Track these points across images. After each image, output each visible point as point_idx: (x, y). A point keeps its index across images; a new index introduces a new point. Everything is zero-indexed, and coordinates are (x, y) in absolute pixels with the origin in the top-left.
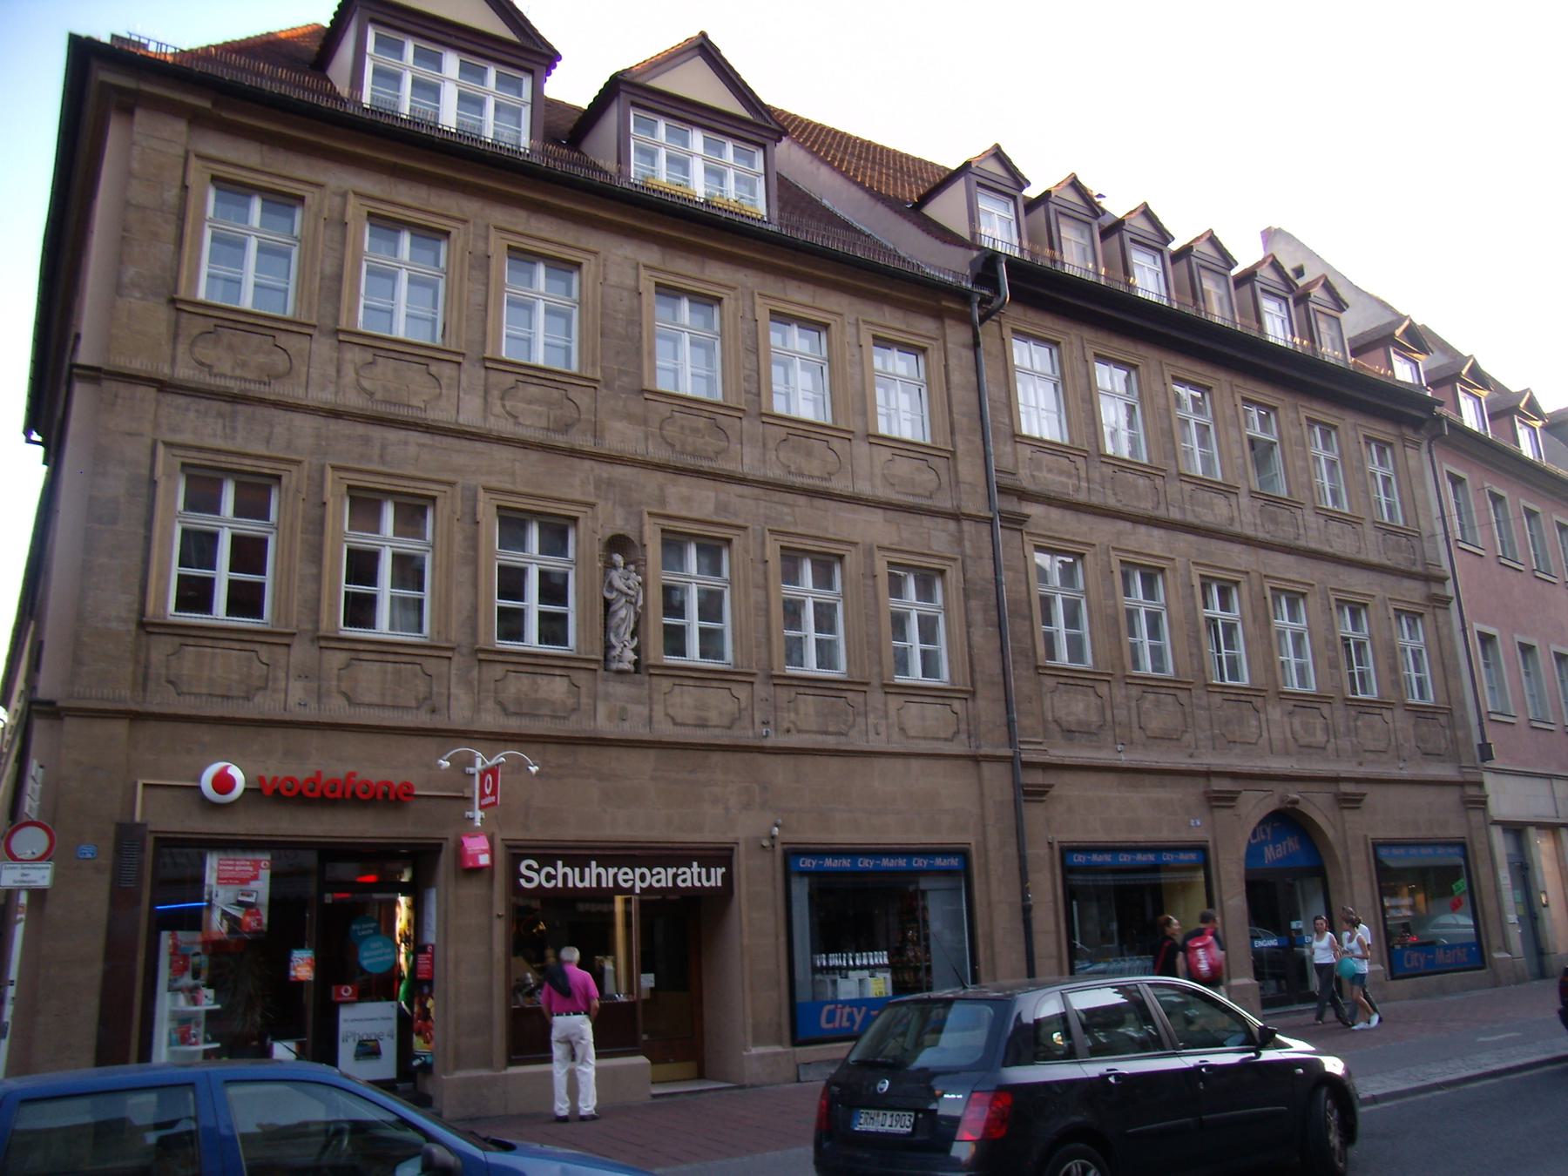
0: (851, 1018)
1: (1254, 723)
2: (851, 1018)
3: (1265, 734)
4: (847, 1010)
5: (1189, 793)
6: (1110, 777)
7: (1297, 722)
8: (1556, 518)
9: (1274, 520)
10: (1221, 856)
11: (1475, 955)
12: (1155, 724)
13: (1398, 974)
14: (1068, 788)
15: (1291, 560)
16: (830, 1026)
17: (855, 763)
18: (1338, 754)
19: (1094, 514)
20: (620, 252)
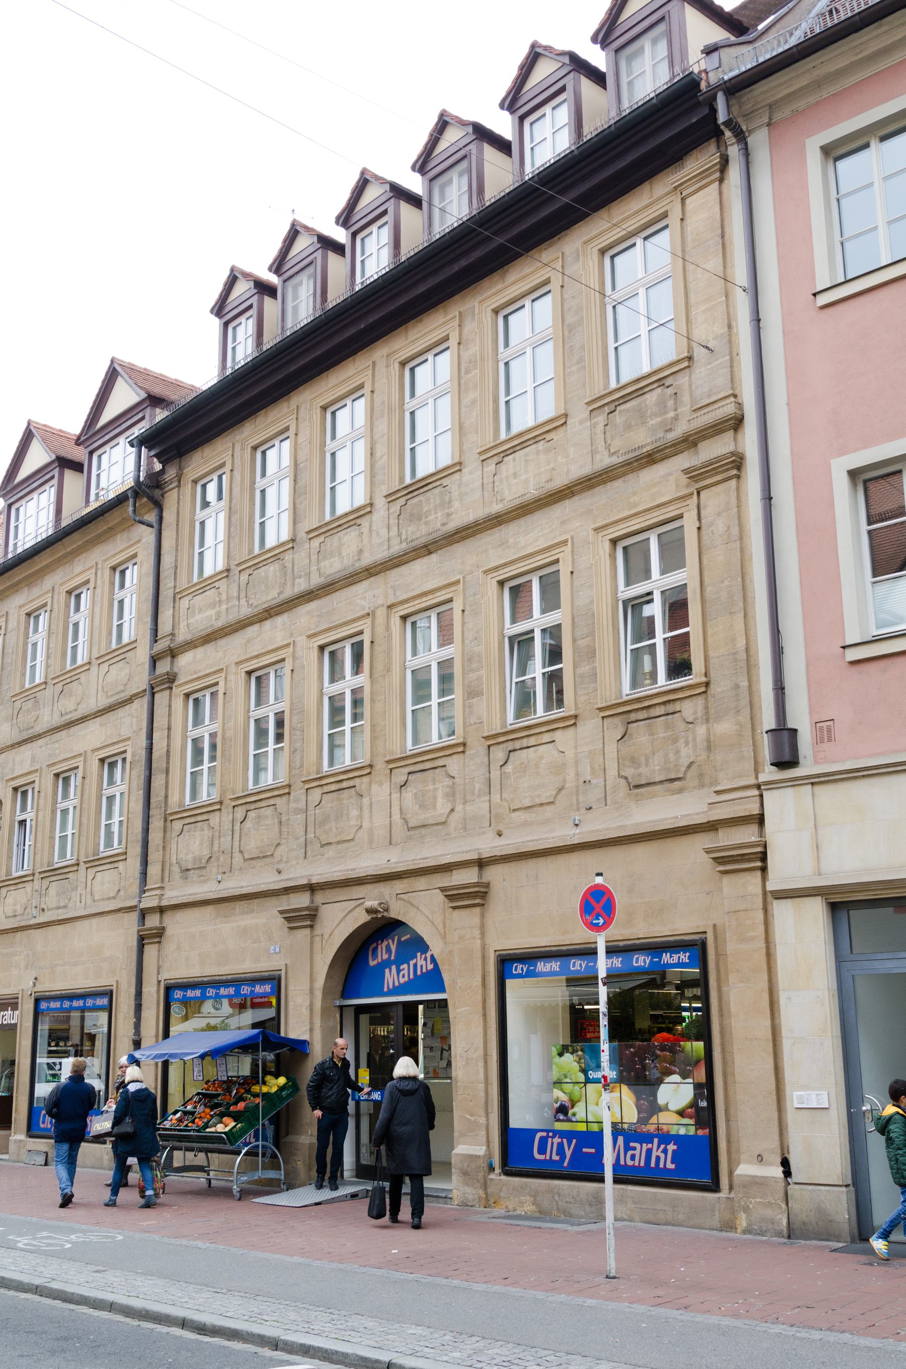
0: (561, 1151)
1: (354, 813)
2: (561, 1151)
3: (366, 825)
4: (557, 1140)
5: (267, 918)
6: (209, 909)
7: (409, 795)
8: (13, 606)
9: (416, 517)
10: (291, 988)
11: (699, 1163)
12: (252, 846)
13: (514, 1167)
14: (178, 927)
15: (419, 566)
16: (542, 1157)
17: (68, 926)
18: (465, 827)
19: (604, 482)
20: (13, 606)
